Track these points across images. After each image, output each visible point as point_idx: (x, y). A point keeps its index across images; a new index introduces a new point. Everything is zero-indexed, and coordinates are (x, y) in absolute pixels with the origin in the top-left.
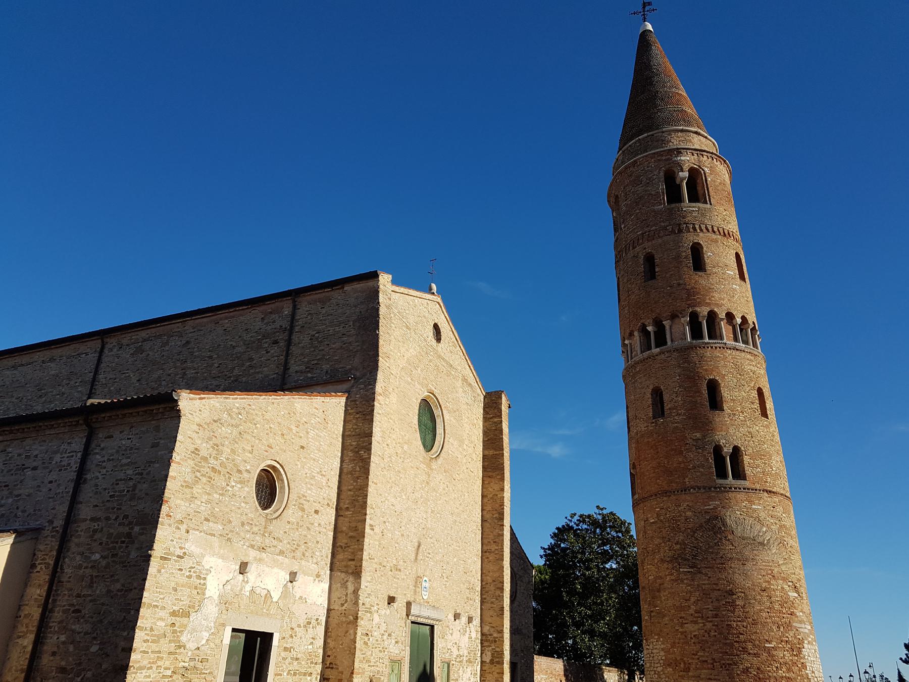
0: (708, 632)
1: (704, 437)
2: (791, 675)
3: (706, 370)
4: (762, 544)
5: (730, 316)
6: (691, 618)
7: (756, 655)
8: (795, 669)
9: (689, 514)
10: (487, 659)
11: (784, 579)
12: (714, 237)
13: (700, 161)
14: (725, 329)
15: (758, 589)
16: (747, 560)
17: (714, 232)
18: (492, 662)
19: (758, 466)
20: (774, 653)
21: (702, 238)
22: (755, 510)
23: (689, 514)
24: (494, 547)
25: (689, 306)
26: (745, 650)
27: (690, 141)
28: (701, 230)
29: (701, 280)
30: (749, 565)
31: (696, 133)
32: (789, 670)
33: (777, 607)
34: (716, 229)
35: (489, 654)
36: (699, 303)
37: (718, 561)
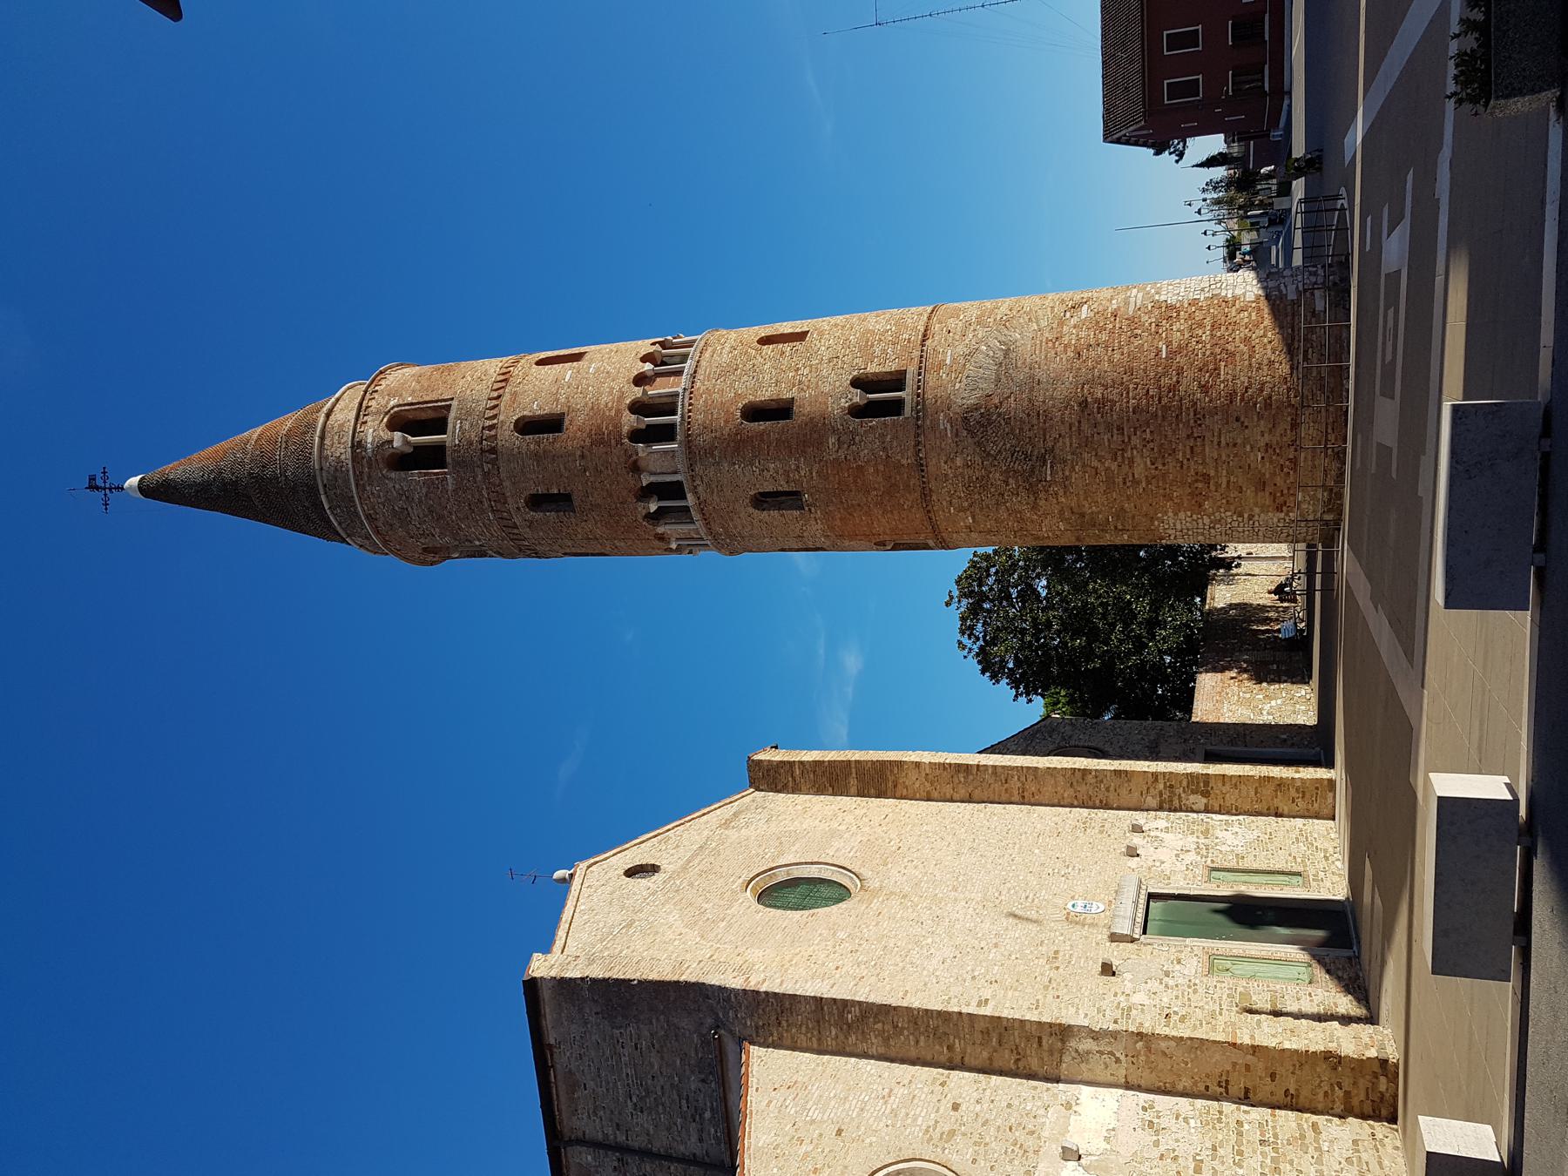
0: (1146, 442)
1: (834, 431)
2: (1208, 322)
3: (726, 422)
4: (1007, 353)
5: (640, 380)
6: (1125, 468)
7: (1180, 371)
8: (1199, 316)
9: (959, 461)
10: (1201, 801)
11: (1061, 323)
12: (506, 398)
13: (378, 412)
14: (661, 388)
15: (1077, 364)
16: (1032, 377)
17: (499, 397)
18: (1206, 794)
19: (884, 351)
20: (1175, 345)
21: (509, 415)
22: (954, 360)
23: (959, 461)
24: (1015, 784)
25: (619, 442)
26: (1173, 389)
27: (342, 425)
28: (495, 417)
29: (577, 424)
30: (1040, 374)
31: (328, 416)
32: (1201, 325)
33: (1104, 337)
34: (495, 394)
35: (1193, 798)
36: (615, 426)
37: (1035, 421)
